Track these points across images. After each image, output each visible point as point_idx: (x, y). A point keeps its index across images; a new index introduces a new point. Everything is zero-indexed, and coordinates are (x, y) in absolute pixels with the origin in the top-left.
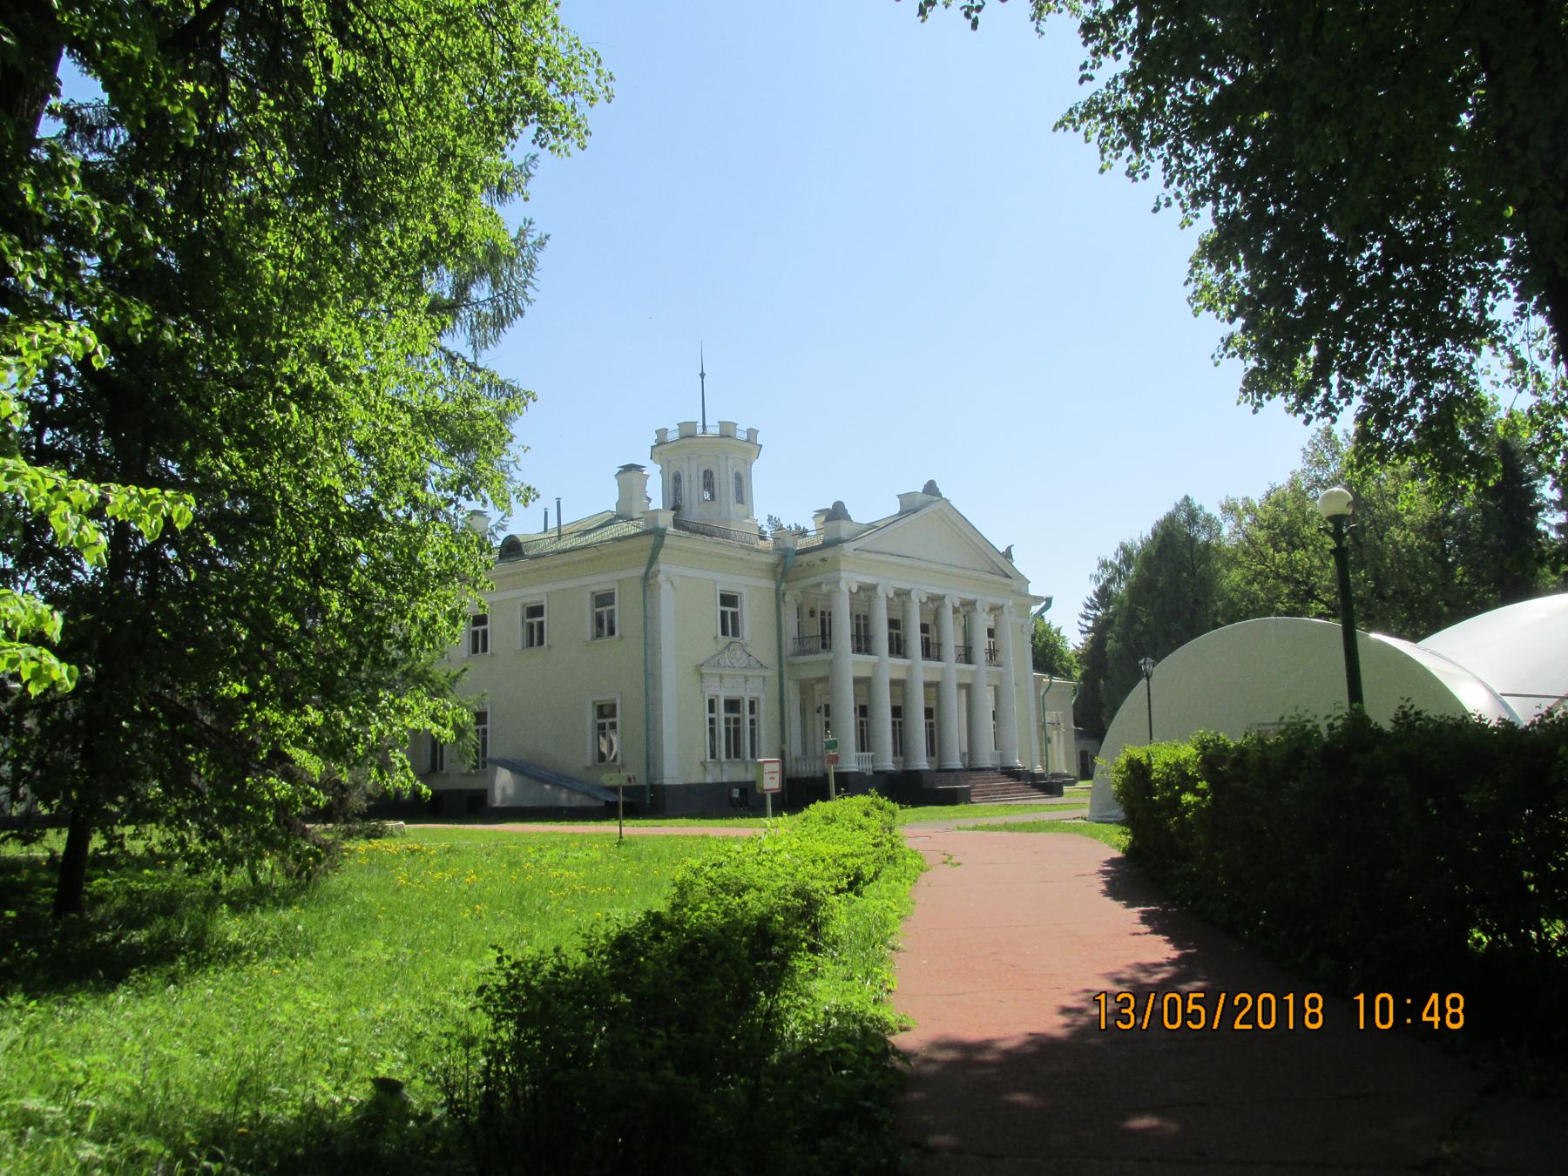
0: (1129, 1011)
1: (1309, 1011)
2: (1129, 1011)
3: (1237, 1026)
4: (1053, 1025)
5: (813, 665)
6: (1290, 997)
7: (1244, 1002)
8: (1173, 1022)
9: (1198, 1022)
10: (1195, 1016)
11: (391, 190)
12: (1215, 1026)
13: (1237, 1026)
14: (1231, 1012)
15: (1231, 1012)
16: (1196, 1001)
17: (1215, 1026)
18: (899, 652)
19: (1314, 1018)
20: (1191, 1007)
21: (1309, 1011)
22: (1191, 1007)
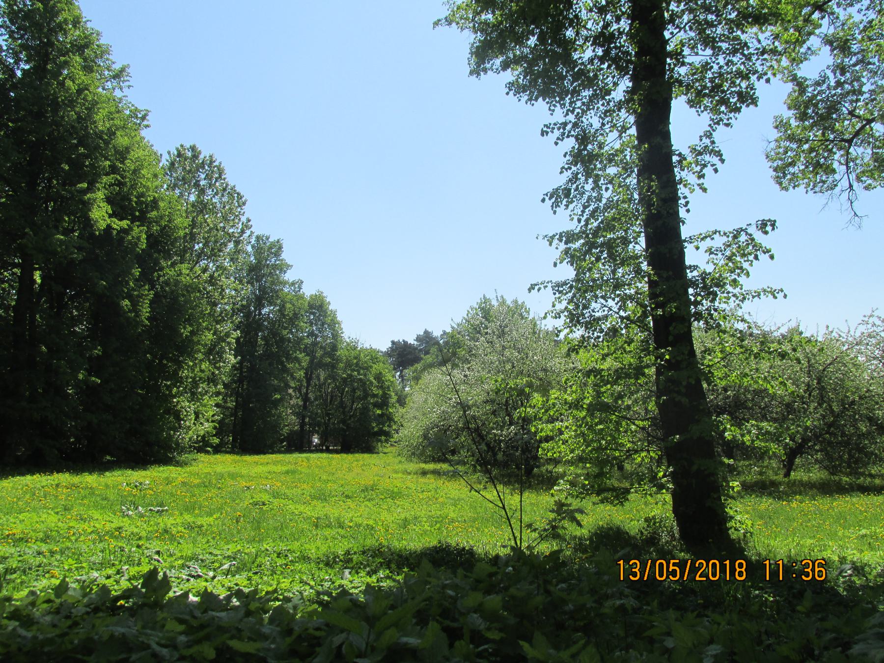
0: (637, 570)
1: (738, 570)
2: (809, 570)
3: (698, 578)
4: (297, 586)
6: (727, 562)
9: (675, 576)
10: (674, 573)
11: (821, 415)
12: (645, 578)
13: (698, 578)
14: (694, 570)
15: (694, 570)
16: (674, 564)
17: (645, 578)
20: (671, 568)
21: (738, 570)
22: (671, 568)
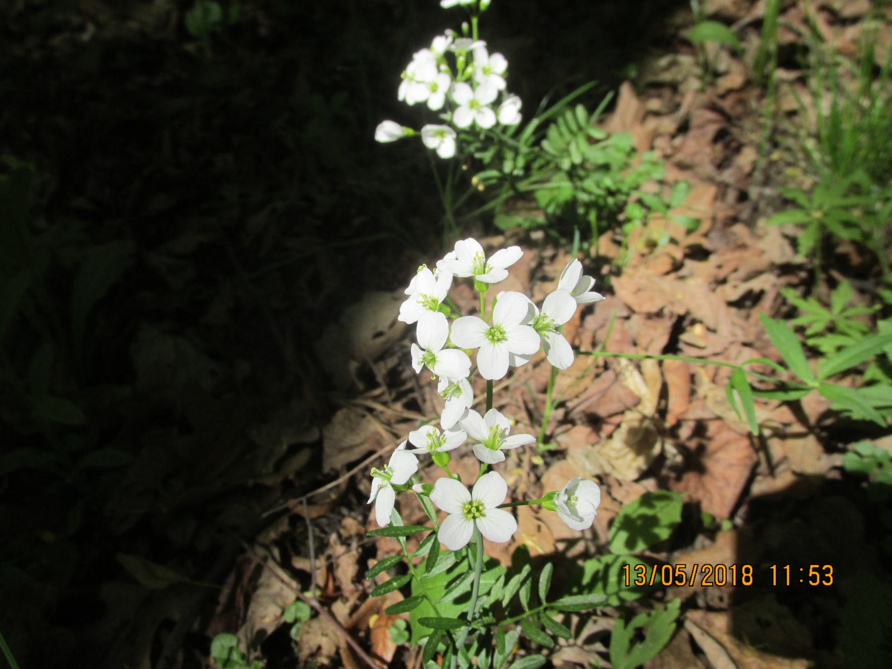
0: (830, 575)
1: (745, 575)
2: (830, 575)
19: (747, 579)
21: (745, 575)
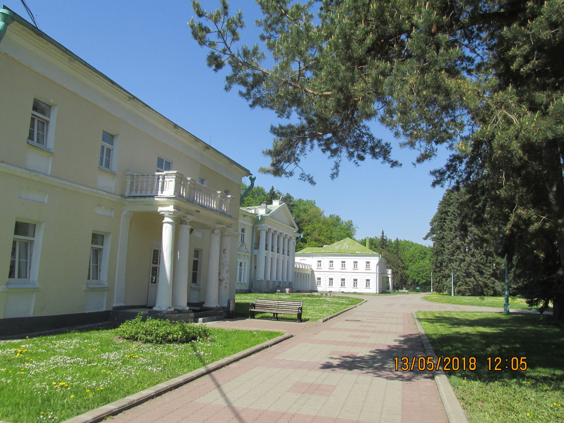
0: (406, 364)
1: (471, 364)
2: (406, 364)
3: (496, 369)
5: (255, 252)
7: (447, 360)
8: (515, 368)
13: (496, 369)
16: (523, 360)
18: (198, 251)
19: (472, 367)
20: (521, 362)
21: (471, 364)
